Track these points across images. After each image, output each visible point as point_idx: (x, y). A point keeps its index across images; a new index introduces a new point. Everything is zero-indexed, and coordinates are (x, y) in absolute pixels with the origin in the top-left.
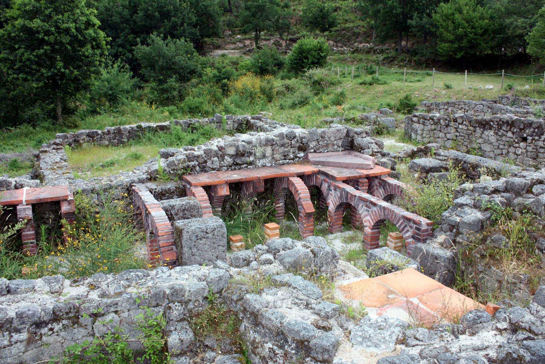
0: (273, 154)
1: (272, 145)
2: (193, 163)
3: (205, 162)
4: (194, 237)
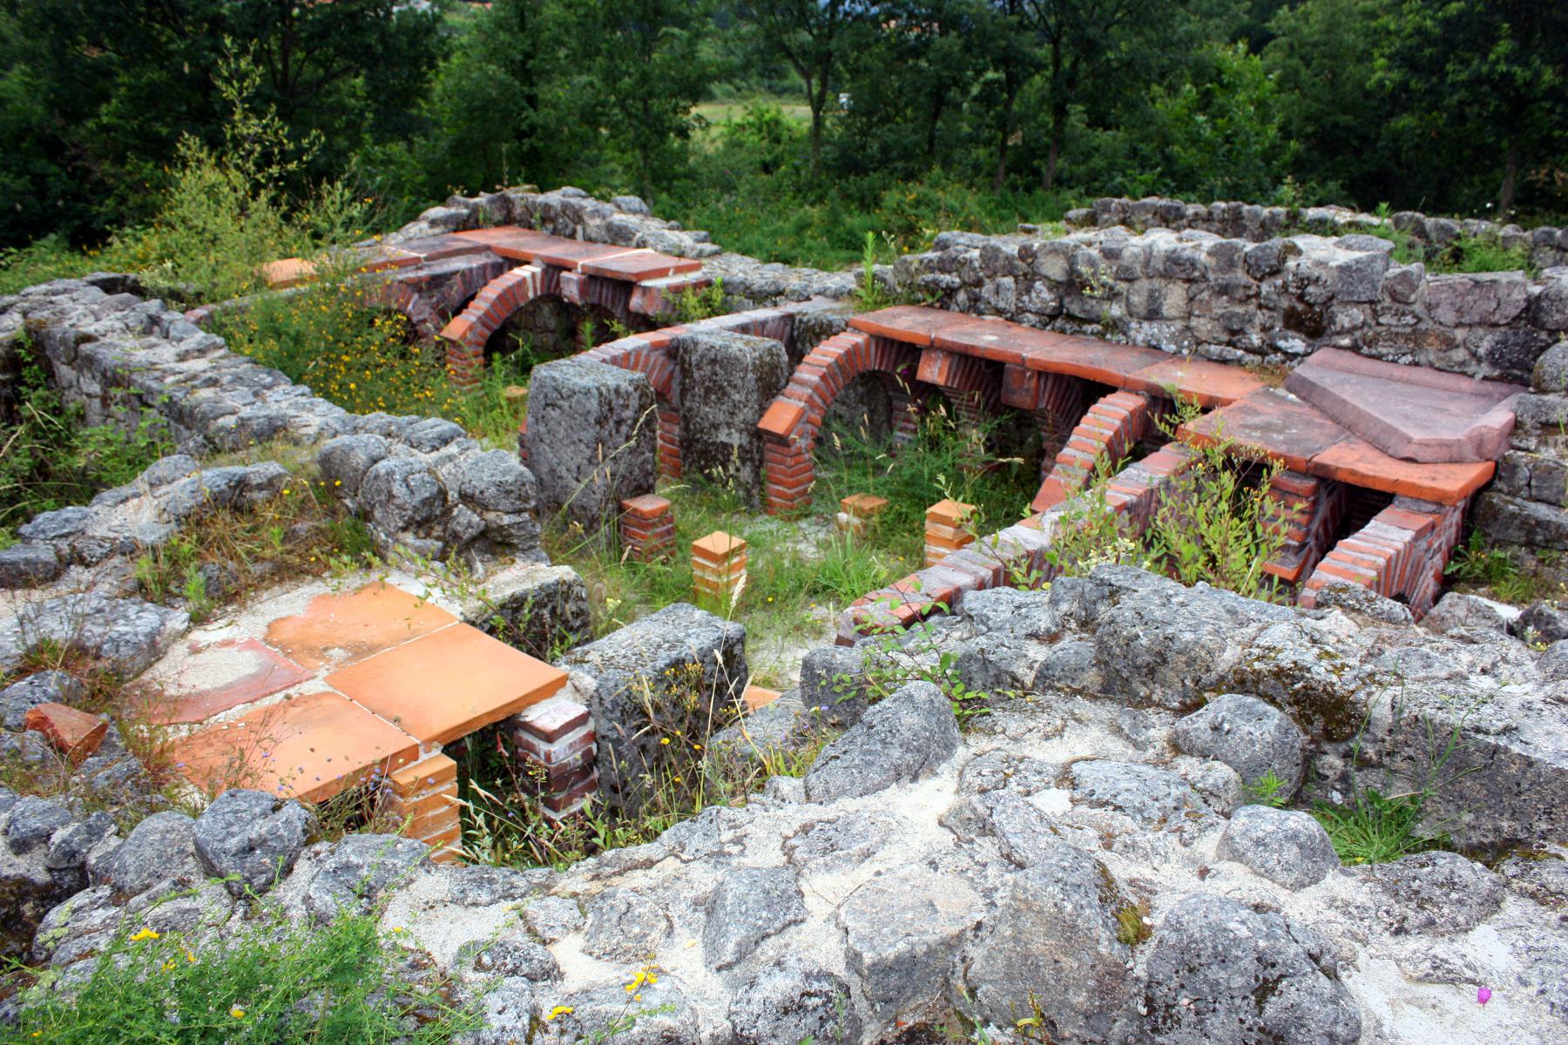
0: (1190, 315)
1: (1189, 281)
3: (979, 283)
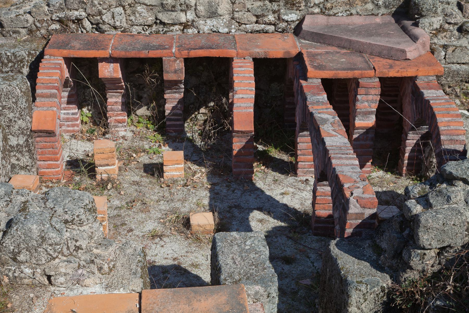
2: (76, 13)
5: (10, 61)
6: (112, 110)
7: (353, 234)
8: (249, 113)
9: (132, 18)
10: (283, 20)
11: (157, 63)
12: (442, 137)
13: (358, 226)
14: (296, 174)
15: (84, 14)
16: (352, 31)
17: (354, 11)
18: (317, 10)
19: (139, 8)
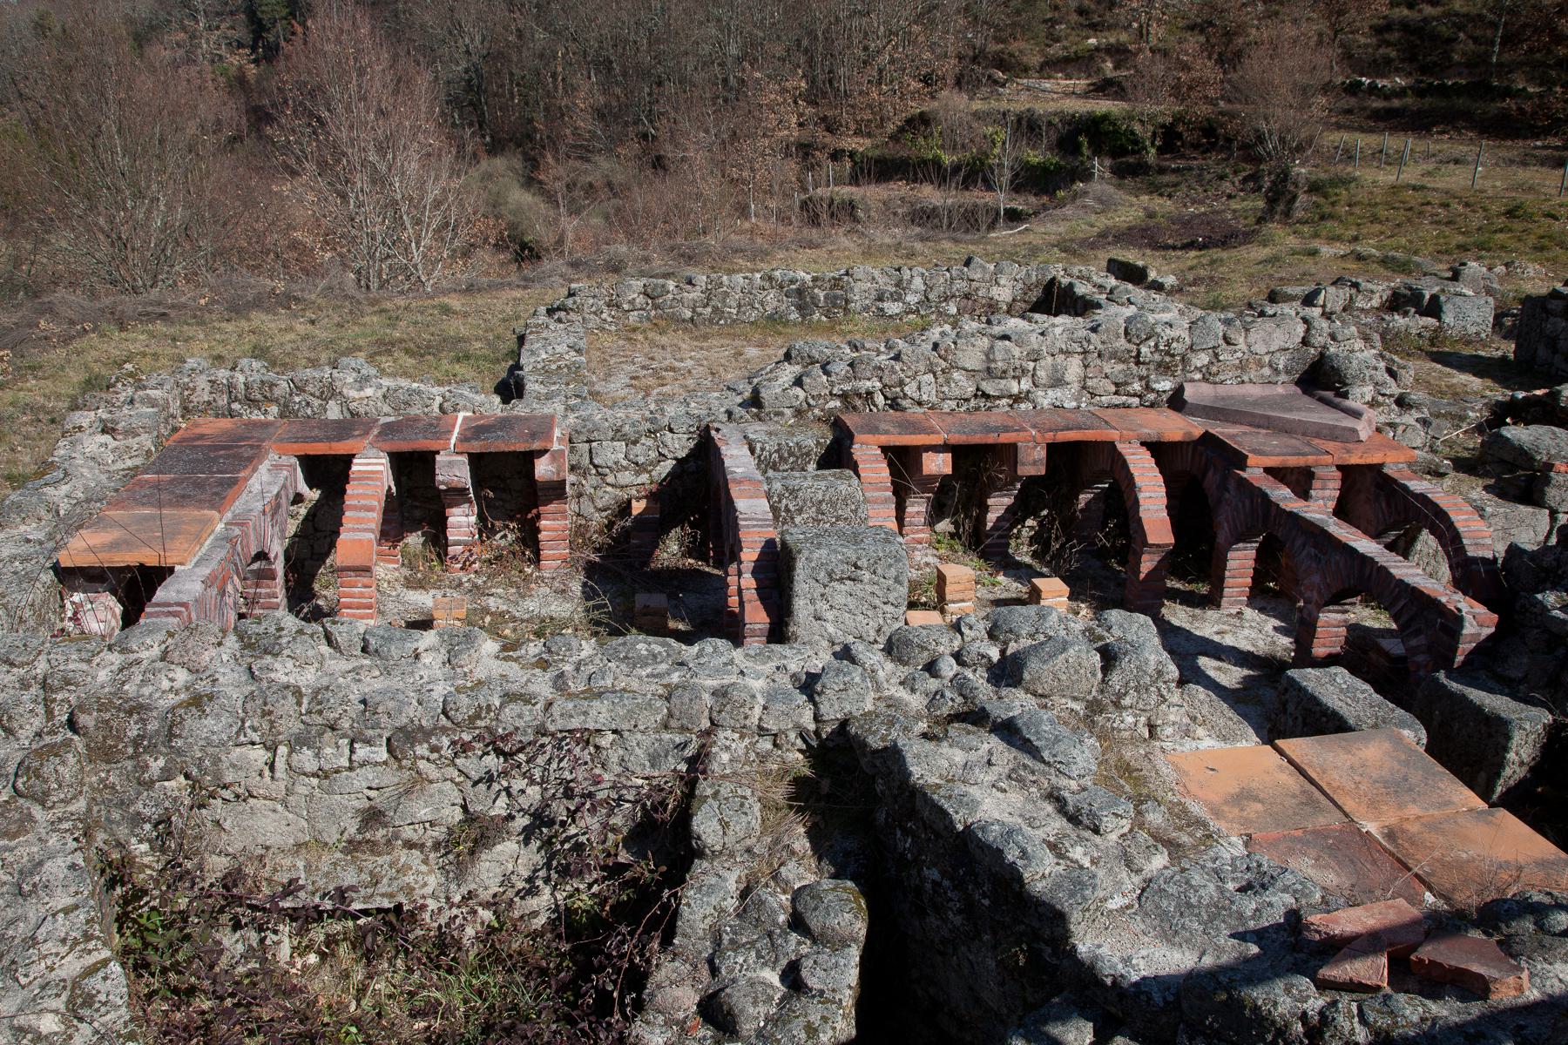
2: (868, 384)
4: (823, 574)
5: (791, 454)
6: (911, 524)
7: (1464, 663)
8: (1162, 520)
9: (945, 389)
10: (1153, 390)
11: (1012, 449)
12: (1465, 541)
13: (1472, 652)
14: (1218, 606)
15: (878, 385)
16: (1255, 403)
17: (1246, 378)
18: (1198, 376)
19: (956, 375)
